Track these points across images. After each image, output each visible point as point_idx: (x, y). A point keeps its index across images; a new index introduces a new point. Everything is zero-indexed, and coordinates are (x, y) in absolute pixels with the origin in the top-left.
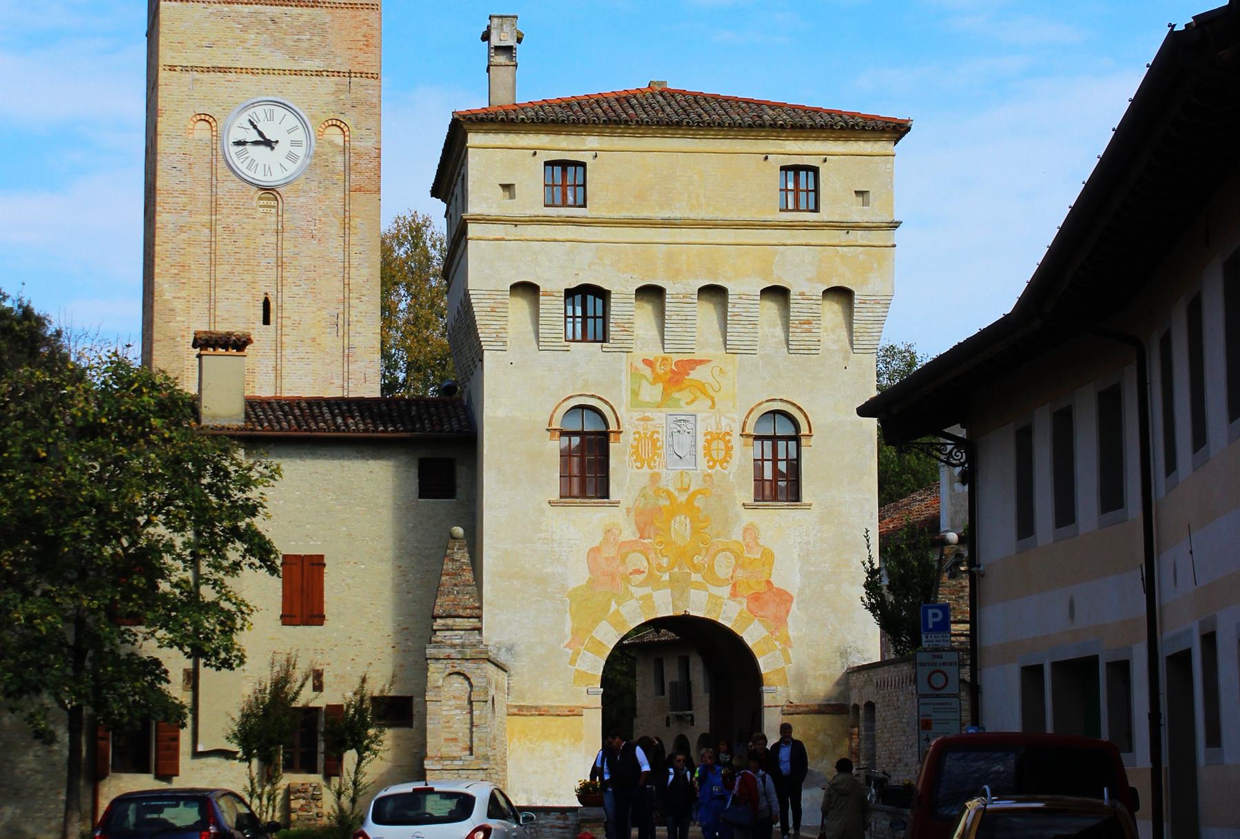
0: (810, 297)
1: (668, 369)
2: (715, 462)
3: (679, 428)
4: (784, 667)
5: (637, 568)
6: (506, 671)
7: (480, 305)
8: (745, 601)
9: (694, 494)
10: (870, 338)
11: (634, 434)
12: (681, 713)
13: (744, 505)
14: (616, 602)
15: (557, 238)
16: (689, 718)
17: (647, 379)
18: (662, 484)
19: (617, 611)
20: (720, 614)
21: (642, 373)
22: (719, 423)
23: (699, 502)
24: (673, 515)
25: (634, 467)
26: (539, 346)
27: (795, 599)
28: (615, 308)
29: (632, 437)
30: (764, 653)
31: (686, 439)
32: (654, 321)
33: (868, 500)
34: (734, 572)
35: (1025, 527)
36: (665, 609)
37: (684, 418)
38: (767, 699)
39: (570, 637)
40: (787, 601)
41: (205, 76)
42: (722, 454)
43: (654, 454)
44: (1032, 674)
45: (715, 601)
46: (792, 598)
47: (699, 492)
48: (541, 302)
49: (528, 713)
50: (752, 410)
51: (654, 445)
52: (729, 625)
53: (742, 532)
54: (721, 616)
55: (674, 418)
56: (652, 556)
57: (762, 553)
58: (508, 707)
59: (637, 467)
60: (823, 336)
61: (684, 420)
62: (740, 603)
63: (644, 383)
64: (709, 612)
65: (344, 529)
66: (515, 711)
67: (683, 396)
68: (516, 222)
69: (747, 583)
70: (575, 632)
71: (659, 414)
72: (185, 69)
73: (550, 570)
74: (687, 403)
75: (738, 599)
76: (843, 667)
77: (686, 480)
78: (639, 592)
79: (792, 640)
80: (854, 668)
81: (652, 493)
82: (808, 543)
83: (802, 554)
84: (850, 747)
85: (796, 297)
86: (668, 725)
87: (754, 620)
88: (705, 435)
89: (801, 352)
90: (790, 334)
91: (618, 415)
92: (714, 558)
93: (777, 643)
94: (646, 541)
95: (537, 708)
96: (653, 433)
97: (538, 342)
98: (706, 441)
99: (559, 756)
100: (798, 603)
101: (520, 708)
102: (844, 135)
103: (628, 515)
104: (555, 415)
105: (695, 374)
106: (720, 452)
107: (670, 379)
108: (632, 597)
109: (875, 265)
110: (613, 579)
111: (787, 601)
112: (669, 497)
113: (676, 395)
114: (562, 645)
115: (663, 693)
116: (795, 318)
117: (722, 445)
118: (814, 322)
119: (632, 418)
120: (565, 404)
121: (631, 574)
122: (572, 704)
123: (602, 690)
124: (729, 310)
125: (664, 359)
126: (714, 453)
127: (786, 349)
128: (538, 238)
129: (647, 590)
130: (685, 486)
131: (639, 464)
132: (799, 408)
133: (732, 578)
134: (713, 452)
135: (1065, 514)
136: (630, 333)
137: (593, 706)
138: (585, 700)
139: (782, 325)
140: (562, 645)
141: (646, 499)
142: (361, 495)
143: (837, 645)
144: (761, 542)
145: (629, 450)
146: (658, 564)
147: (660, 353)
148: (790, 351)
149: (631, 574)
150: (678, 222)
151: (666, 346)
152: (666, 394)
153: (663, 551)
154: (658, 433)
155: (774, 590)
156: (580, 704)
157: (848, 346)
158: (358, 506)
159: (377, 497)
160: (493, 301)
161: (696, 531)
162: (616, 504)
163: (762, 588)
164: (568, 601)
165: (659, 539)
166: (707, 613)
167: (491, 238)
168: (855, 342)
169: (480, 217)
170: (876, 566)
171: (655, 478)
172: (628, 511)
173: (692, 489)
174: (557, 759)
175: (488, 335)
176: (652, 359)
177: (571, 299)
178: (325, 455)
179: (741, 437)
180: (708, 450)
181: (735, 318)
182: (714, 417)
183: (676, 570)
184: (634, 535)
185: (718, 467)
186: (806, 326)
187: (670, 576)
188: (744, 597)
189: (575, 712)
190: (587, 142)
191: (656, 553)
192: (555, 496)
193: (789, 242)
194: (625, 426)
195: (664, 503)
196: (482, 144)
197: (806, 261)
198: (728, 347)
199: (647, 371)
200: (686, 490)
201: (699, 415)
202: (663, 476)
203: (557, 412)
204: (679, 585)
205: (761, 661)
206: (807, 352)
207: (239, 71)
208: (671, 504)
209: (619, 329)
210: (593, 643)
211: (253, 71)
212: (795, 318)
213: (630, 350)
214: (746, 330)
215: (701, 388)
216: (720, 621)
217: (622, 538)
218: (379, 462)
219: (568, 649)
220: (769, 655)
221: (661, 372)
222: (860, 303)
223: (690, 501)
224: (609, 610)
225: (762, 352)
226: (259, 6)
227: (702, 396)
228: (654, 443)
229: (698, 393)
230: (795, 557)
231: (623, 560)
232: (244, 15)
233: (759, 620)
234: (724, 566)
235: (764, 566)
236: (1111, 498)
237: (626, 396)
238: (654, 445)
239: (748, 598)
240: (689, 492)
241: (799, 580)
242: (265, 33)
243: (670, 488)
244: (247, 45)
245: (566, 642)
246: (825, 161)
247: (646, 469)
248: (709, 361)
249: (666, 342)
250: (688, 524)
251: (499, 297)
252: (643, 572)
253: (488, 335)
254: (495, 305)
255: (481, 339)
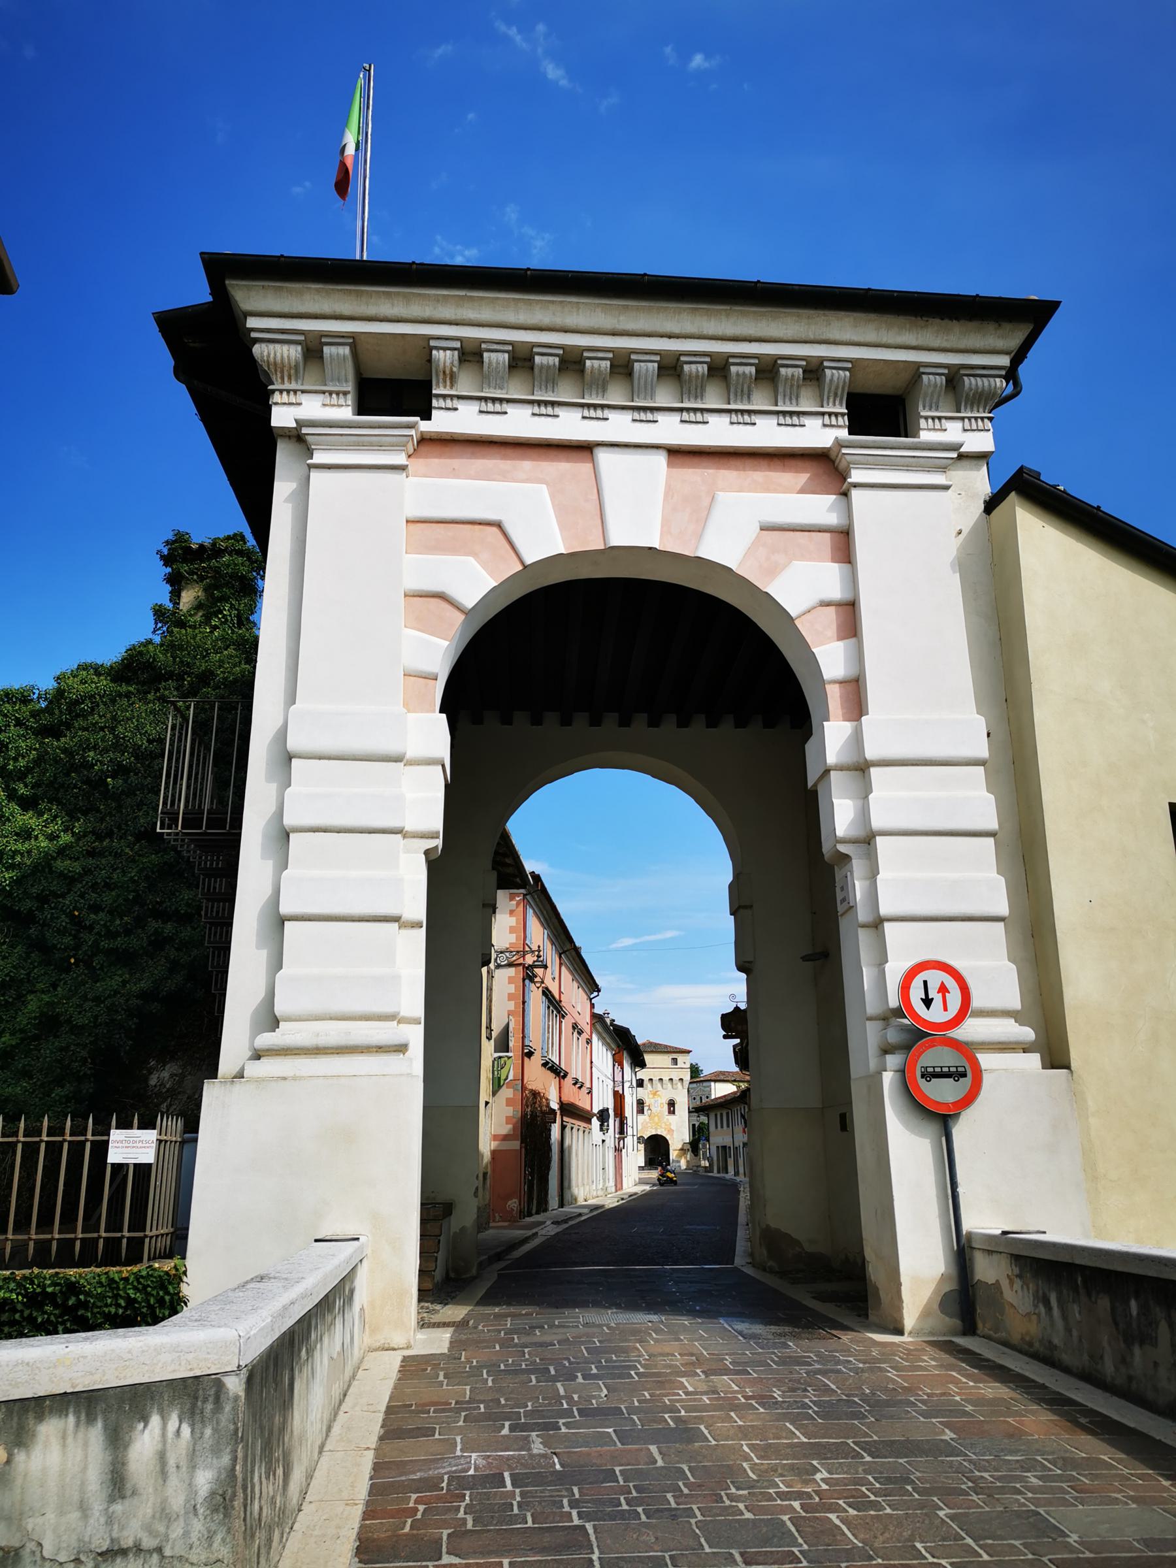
35: (716, 1127)
36: (654, 1133)
44: (718, 1147)
135: (722, 1127)
170: (484, 970)
177: (306, 437)
204: (656, 1129)
234: (663, 1126)
236: (728, 1126)
255: (252, 323)
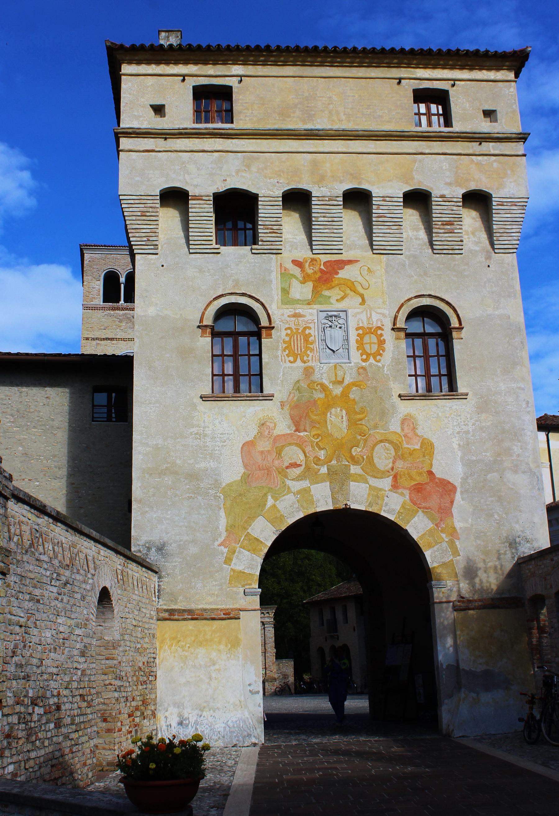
0: (450, 199)
1: (317, 269)
2: (368, 355)
3: (330, 324)
4: (452, 560)
5: (293, 461)
6: (156, 572)
7: (131, 209)
8: (407, 492)
9: (349, 386)
10: (510, 238)
11: (286, 329)
12: (332, 634)
13: (400, 396)
14: (272, 497)
15: (206, 149)
16: (336, 637)
17: (297, 278)
18: (316, 376)
19: (274, 506)
20: (382, 506)
21: (291, 272)
22: (369, 318)
23: (354, 394)
24: (328, 407)
25: (287, 361)
26: (189, 249)
27: (459, 490)
28: (263, 211)
29: (284, 333)
30: (430, 546)
31: (338, 334)
32: (302, 227)
33: (523, 389)
34: (394, 463)
37: (335, 313)
38: (438, 594)
39: (224, 535)
40: (450, 491)
41: (103, 342)
42: (375, 348)
43: (307, 348)
45: (376, 492)
46: (455, 488)
47: (354, 384)
48: (190, 206)
49: (180, 618)
50: (402, 305)
51: (306, 340)
52: (391, 517)
53: (399, 422)
54: (384, 508)
55: (325, 314)
56: (308, 449)
57: (422, 443)
58: (158, 610)
59: (289, 361)
60: (465, 238)
61: (335, 316)
62: (402, 494)
63: (294, 282)
64: (370, 505)
65: (20, 448)
66: (166, 615)
67: (334, 294)
68: (165, 135)
69: (408, 474)
70: (230, 529)
71: (310, 311)
72: (93, 339)
73: (203, 465)
74: (337, 300)
75: (400, 491)
76: (513, 558)
77: (340, 373)
78: (296, 486)
79: (458, 531)
80: (524, 557)
81: (306, 386)
82: (467, 432)
83: (462, 443)
84: (530, 643)
85: (437, 199)
86: (326, 640)
87: (418, 511)
88: (357, 329)
89: (445, 252)
90: (434, 235)
91: (269, 312)
92: (373, 449)
93: (444, 535)
94: (302, 434)
95: (190, 612)
96: (305, 329)
97: (188, 245)
98: (359, 335)
99: (214, 665)
100: (462, 493)
101: (172, 612)
102: (469, 63)
103: (282, 409)
104: (207, 313)
105: (344, 274)
106: (372, 345)
107: (320, 278)
108: (289, 491)
109: (509, 172)
110: (269, 473)
111: (450, 491)
112: (324, 390)
113: (326, 293)
114: (216, 543)
115: (323, 625)
116: (437, 219)
117: (374, 339)
118: (455, 223)
119: (283, 315)
120: (215, 302)
121: (287, 468)
122: (228, 607)
123: (260, 590)
124: (374, 211)
125: (313, 260)
126: (367, 347)
127: (430, 250)
128: (188, 149)
129: (305, 484)
130: (339, 379)
131: (291, 359)
132: (448, 303)
133: (392, 469)
134: (365, 346)
136: (278, 235)
137: (250, 608)
138: (242, 602)
139: (425, 228)
140: (216, 543)
141: (300, 393)
142: (37, 418)
143: (505, 535)
144: (419, 432)
145: (282, 346)
146: (316, 457)
147: (309, 254)
148: (435, 251)
149: (287, 468)
150: (321, 132)
151: (314, 247)
152: (316, 291)
153: (320, 443)
154: (310, 328)
155: (437, 480)
156: (236, 606)
157: (489, 247)
158: (34, 427)
159: (53, 420)
160: (143, 206)
161: (353, 423)
162: (270, 397)
163: (425, 479)
164: (222, 497)
165: (314, 432)
166: (368, 506)
167: (142, 149)
168: (496, 242)
169: (130, 131)
171: (308, 372)
172: (282, 404)
173: (346, 382)
174: (212, 668)
175: (139, 239)
176: (301, 260)
178: (5, 382)
179: (393, 331)
180: (360, 345)
181: (380, 219)
182: (365, 312)
183: (334, 462)
184: (289, 427)
185: (372, 360)
186: (449, 227)
187: (328, 469)
188: (407, 489)
189: (231, 615)
190: (233, 70)
191: (312, 446)
192: (207, 391)
193: (427, 151)
194: (276, 322)
195: (319, 395)
196: (134, 72)
197: (444, 168)
198: (374, 247)
199: (297, 271)
200: (341, 382)
201: (350, 312)
202: (317, 370)
203: (208, 310)
205: (428, 554)
206: (451, 252)
207: (118, 339)
208: (326, 396)
209: (268, 231)
210: (250, 540)
211: (124, 340)
212: (437, 219)
213: (279, 251)
214: (392, 231)
215: (351, 286)
216: (383, 514)
217: (277, 432)
218: (56, 389)
219: (222, 547)
220: (435, 548)
221: (310, 271)
222: (498, 205)
223: (345, 394)
224: (265, 505)
225: (407, 253)
226: (127, 311)
227: (352, 293)
228: (306, 338)
229: (348, 291)
230: (455, 446)
231: (279, 454)
232: (120, 315)
233: (423, 512)
235: (424, 456)
237: (277, 295)
238: (306, 340)
239: (409, 489)
240: (343, 385)
241: (460, 469)
242: (129, 323)
243: (324, 381)
244: (121, 328)
245: (220, 540)
246: (453, 85)
247: (299, 363)
248: (357, 261)
249: (314, 243)
250: (344, 416)
251: (149, 202)
252: (300, 465)
253: (139, 239)
254: (145, 210)
